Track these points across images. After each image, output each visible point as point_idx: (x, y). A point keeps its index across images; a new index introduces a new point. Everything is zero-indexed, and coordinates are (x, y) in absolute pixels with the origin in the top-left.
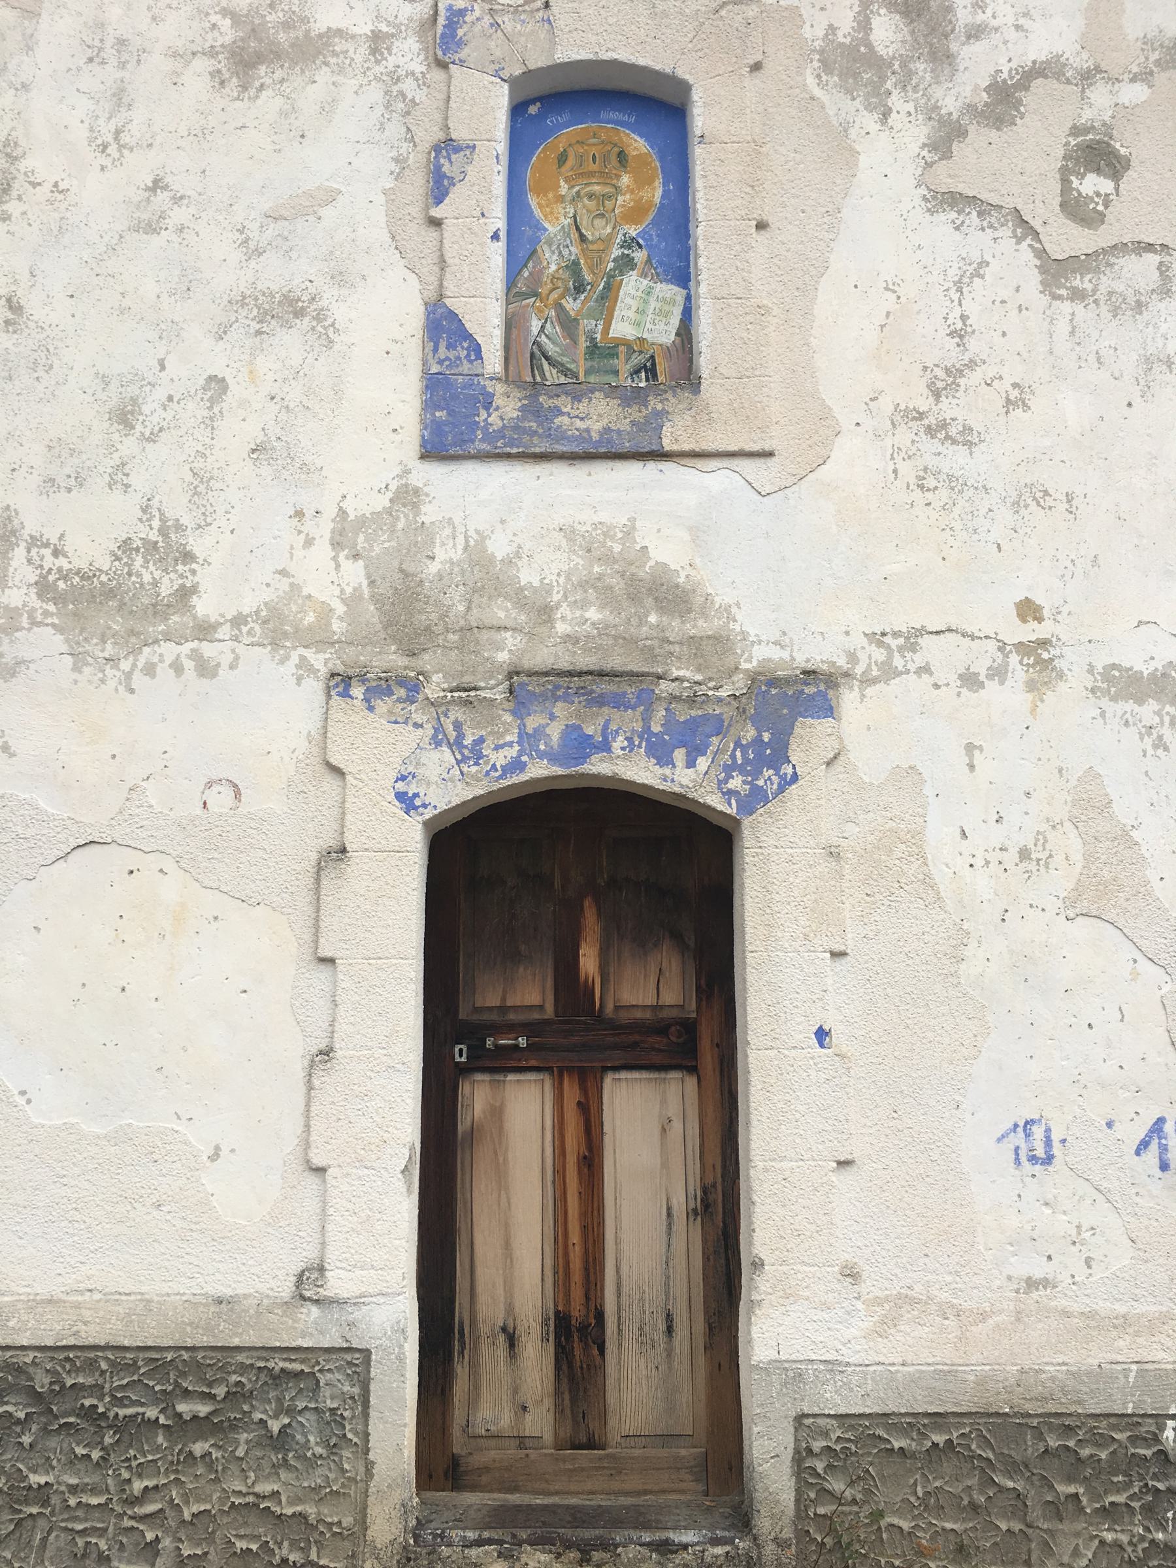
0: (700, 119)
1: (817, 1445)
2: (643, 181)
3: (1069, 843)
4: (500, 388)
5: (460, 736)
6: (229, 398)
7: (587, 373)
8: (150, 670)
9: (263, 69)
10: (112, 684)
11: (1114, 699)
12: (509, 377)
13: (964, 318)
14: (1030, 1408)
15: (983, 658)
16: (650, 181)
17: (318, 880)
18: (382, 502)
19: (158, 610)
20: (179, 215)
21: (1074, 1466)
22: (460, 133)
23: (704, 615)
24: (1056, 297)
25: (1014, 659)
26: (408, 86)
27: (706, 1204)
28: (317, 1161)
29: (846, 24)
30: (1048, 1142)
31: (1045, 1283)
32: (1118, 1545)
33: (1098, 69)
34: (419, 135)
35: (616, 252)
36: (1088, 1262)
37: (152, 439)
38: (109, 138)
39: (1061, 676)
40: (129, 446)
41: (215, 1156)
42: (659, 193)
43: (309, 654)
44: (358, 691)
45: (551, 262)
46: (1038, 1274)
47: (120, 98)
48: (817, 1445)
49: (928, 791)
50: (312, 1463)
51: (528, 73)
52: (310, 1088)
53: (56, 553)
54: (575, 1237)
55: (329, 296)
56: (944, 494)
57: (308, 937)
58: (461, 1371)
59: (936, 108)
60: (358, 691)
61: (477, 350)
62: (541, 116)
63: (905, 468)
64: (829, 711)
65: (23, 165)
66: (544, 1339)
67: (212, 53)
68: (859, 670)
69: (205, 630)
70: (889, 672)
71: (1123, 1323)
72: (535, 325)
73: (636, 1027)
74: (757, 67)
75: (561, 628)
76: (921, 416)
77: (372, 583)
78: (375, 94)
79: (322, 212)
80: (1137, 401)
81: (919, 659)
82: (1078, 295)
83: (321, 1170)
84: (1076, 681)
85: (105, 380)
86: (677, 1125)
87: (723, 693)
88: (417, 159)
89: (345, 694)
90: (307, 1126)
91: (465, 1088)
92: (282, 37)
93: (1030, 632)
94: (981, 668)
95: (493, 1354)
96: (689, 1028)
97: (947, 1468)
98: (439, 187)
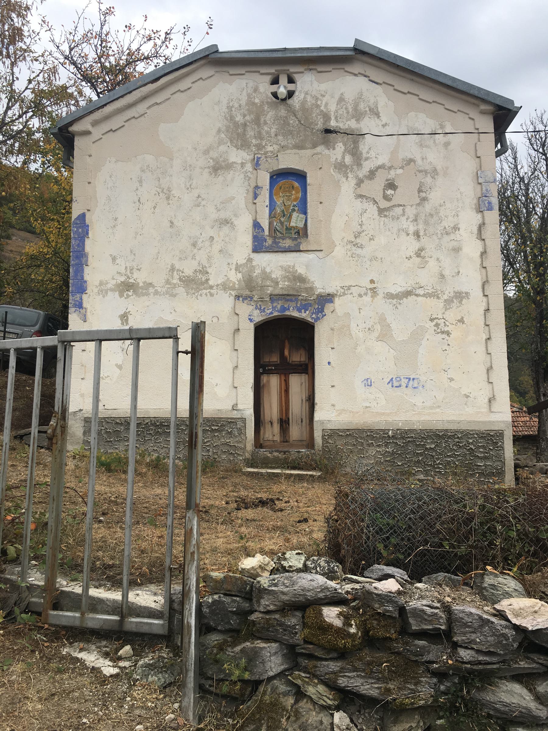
0: (309, 180)
1: (326, 434)
2: (297, 192)
3: (378, 327)
4: (268, 238)
5: (261, 307)
6: (215, 241)
7: (286, 233)
8: (201, 295)
9: (219, 171)
10: (194, 298)
11: (388, 299)
12: (270, 235)
13: (362, 221)
14: (365, 428)
15: (363, 291)
16: (299, 193)
17: (234, 335)
18: (245, 261)
19: (202, 283)
20: (203, 203)
21: (373, 438)
22: (260, 184)
23: (308, 283)
24: (381, 217)
25: (369, 291)
26: (249, 174)
27: (309, 399)
28: (236, 386)
29: (340, 158)
30: (371, 382)
31: (369, 407)
32: (380, 451)
33: (392, 166)
34: (251, 184)
35: (292, 208)
36: (377, 403)
37: (200, 249)
38: (189, 186)
39: (378, 294)
40: (195, 251)
41: (217, 385)
42: (300, 195)
43: (231, 292)
44: (241, 299)
45: (278, 210)
46: (368, 405)
47: (190, 178)
48: (326, 434)
49: (351, 317)
50: (236, 437)
51: (273, 171)
52: (234, 373)
53: (182, 272)
54: (284, 404)
55: (234, 219)
56: (356, 258)
57: (232, 346)
58: (262, 429)
59: (358, 176)
60: (241, 299)
61: (263, 230)
62: (276, 178)
63: (348, 253)
64: (332, 302)
65: (172, 192)
66: (278, 423)
67: (209, 168)
68: (338, 294)
69: (211, 287)
70: (344, 294)
71: (383, 414)
72: (275, 224)
73: (296, 365)
74: (321, 168)
75: (280, 286)
76: (352, 242)
77: (243, 278)
78: (242, 176)
79: (232, 201)
80: (396, 238)
81: (350, 291)
82: (385, 216)
83: (236, 387)
84: (381, 295)
85: (190, 238)
86: (304, 384)
87: (312, 299)
88: (251, 190)
89: (238, 299)
90: (233, 380)
91: (262, 377)
92: (223, 164)
93: (372, 286)
94: (362, 293)
95: (268, 426)
96: (306, 365)
97: (349, 438)
98: (256, 196)
